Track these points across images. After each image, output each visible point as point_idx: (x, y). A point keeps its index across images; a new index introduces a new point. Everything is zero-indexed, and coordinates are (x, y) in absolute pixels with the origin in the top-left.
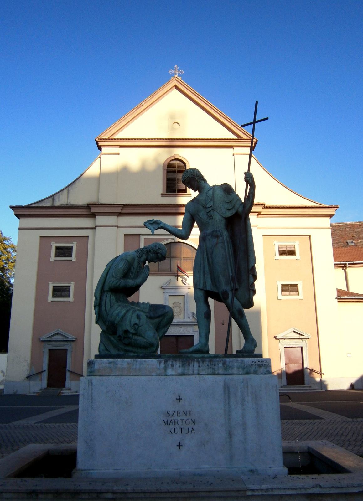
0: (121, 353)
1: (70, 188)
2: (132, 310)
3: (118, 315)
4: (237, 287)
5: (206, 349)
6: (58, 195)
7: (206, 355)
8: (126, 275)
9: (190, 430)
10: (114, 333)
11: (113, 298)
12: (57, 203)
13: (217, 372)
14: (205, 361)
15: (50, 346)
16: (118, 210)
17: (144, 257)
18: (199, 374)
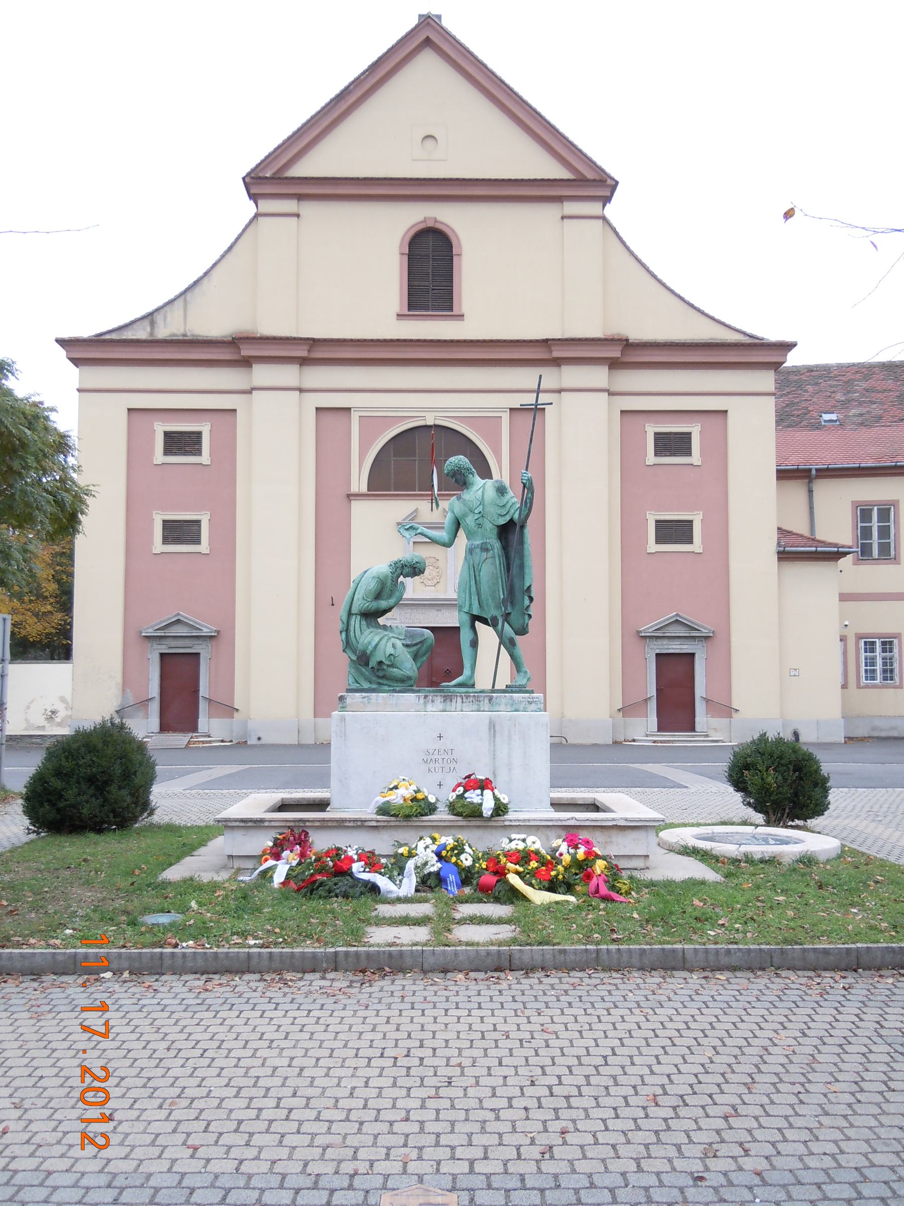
0: (374, 686)
1: (189, 295)
2: (386, 638)
3: (370, 643)
4: (509, 610)
5: (471, 682)
6: (162, 311)
7: (471, 690)
8: (378, 596)
9: (452, 769)
10: (367, 664)
11: (364, 622)
12: (162, 333)
13: (482, 709)
14: (469, 696)
15: (163, 647)
16: (302, 352)
17: (399, 571)
18: (462, 711)
